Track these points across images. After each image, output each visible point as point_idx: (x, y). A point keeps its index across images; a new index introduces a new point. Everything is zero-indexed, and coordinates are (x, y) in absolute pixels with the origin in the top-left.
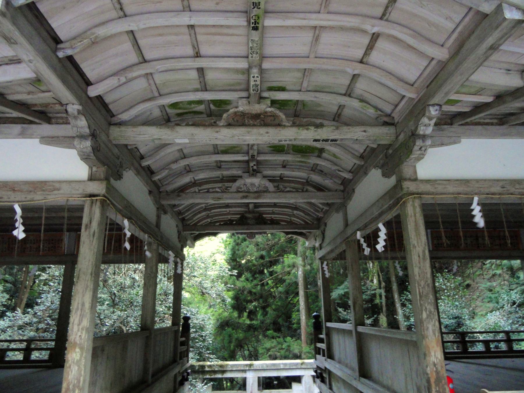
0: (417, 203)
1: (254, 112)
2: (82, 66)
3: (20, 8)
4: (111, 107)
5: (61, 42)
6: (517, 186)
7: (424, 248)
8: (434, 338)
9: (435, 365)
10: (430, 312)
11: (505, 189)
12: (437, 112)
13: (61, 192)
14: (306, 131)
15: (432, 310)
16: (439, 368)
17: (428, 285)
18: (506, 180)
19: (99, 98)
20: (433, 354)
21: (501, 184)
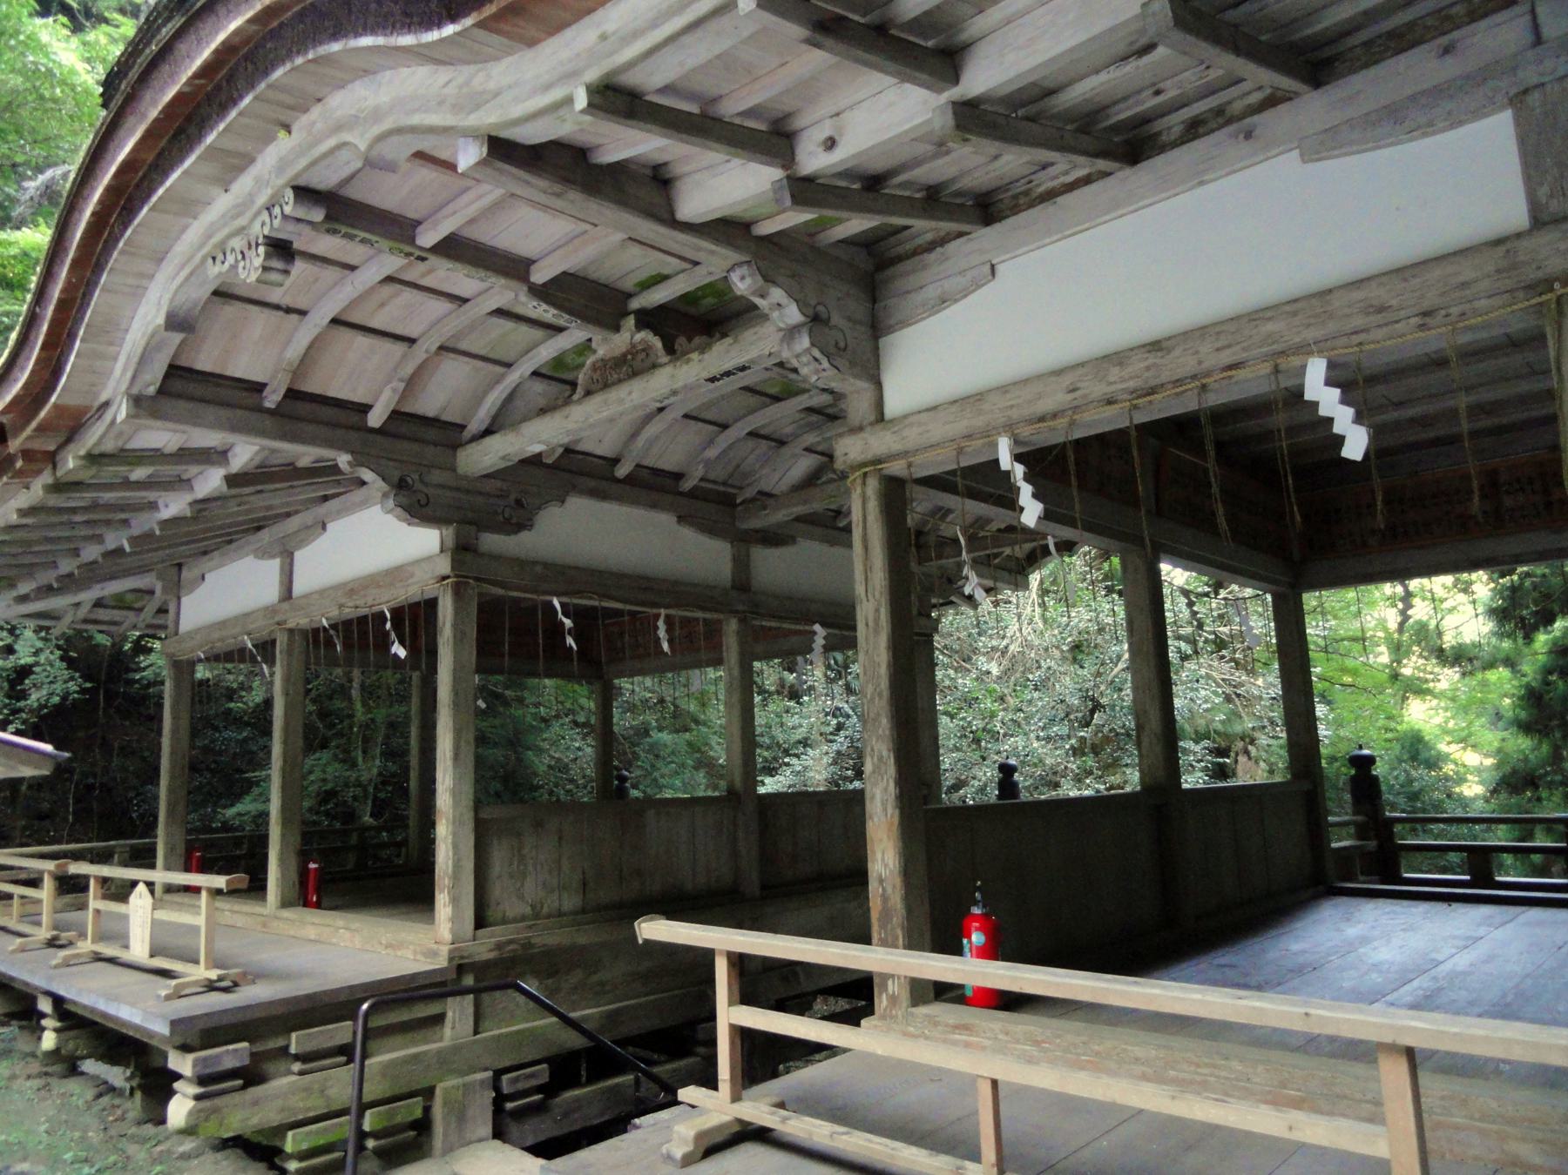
0: (873, 485)
1: (617, 353)
2: (331, 394)
3: (161, 391)
4: (444, 418)
5: (264, 385)
6: (1115, 373)
7: (879, 604)
8: (883, 819)
9: (881, 881)
10: (881, 758)
11: (1077, 394)
12: (748, 281)
13: (414, 580)
14: (685, 367)
15: (885, 753)
16: (889, 890)
17: (880, 695)
18: (1082, 365)
19: (396, 415)
20: (879, 856)
21: (1067, 380)
